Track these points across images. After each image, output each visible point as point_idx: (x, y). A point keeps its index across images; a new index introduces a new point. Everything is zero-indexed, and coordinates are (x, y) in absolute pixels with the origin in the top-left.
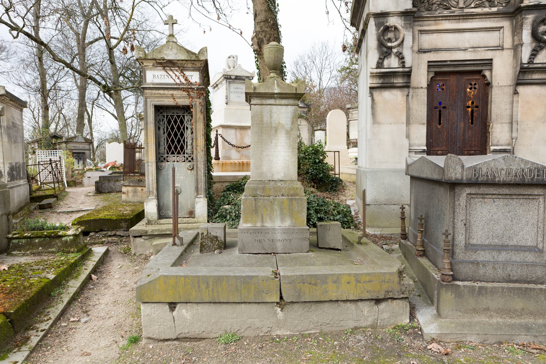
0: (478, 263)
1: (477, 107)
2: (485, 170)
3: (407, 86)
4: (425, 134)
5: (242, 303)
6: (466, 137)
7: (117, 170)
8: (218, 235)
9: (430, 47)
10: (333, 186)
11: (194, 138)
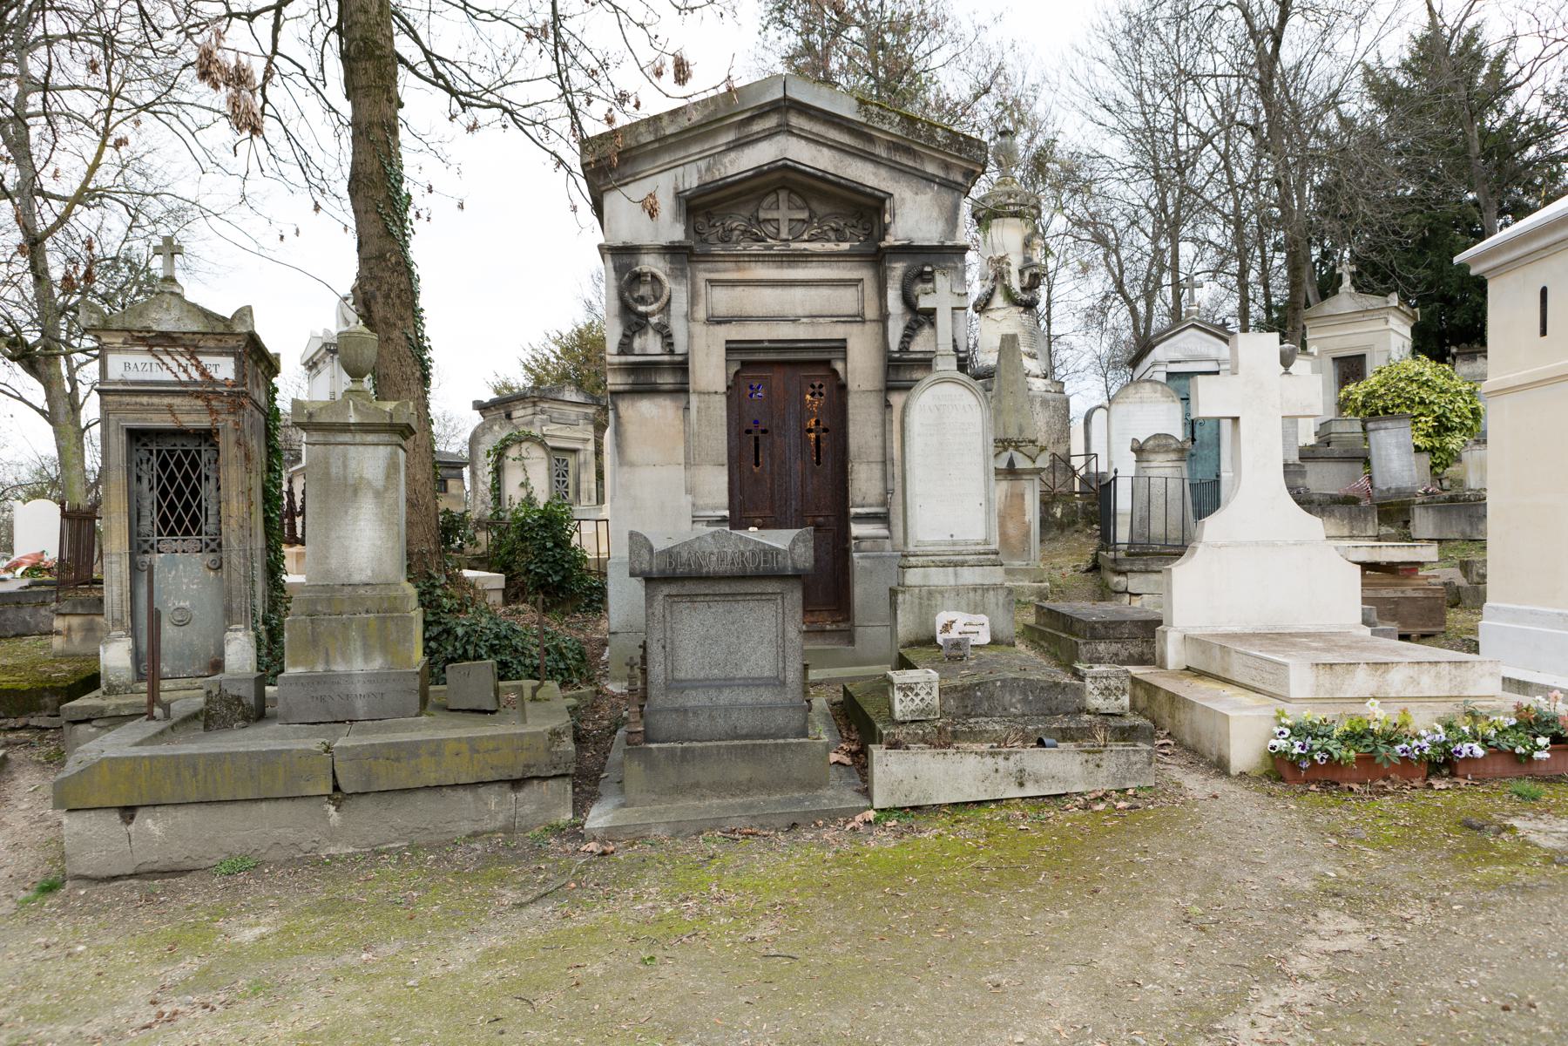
0: (686, 711)
1: (825, 430)
2: (685, 555)
3: (682, 390)
4: (725, 486)
5: (262, 800)
6: (809, 489)
7: (47, 577)
8: (242, 693)
9: (732, 312)
10: (592, 601)
11: (233, 496)
